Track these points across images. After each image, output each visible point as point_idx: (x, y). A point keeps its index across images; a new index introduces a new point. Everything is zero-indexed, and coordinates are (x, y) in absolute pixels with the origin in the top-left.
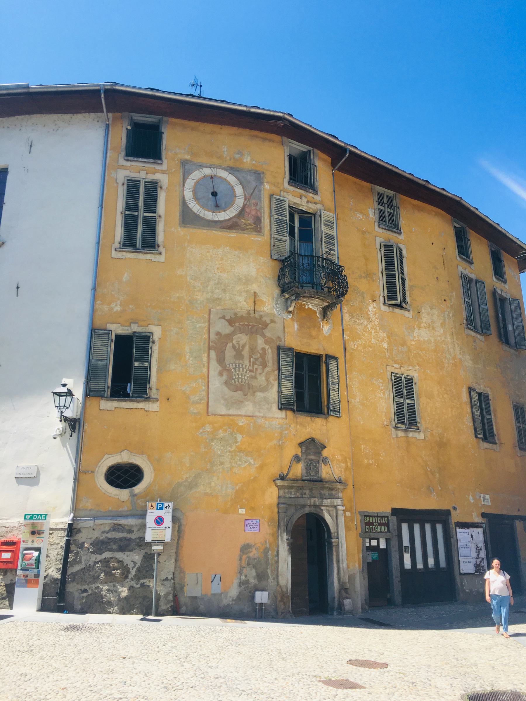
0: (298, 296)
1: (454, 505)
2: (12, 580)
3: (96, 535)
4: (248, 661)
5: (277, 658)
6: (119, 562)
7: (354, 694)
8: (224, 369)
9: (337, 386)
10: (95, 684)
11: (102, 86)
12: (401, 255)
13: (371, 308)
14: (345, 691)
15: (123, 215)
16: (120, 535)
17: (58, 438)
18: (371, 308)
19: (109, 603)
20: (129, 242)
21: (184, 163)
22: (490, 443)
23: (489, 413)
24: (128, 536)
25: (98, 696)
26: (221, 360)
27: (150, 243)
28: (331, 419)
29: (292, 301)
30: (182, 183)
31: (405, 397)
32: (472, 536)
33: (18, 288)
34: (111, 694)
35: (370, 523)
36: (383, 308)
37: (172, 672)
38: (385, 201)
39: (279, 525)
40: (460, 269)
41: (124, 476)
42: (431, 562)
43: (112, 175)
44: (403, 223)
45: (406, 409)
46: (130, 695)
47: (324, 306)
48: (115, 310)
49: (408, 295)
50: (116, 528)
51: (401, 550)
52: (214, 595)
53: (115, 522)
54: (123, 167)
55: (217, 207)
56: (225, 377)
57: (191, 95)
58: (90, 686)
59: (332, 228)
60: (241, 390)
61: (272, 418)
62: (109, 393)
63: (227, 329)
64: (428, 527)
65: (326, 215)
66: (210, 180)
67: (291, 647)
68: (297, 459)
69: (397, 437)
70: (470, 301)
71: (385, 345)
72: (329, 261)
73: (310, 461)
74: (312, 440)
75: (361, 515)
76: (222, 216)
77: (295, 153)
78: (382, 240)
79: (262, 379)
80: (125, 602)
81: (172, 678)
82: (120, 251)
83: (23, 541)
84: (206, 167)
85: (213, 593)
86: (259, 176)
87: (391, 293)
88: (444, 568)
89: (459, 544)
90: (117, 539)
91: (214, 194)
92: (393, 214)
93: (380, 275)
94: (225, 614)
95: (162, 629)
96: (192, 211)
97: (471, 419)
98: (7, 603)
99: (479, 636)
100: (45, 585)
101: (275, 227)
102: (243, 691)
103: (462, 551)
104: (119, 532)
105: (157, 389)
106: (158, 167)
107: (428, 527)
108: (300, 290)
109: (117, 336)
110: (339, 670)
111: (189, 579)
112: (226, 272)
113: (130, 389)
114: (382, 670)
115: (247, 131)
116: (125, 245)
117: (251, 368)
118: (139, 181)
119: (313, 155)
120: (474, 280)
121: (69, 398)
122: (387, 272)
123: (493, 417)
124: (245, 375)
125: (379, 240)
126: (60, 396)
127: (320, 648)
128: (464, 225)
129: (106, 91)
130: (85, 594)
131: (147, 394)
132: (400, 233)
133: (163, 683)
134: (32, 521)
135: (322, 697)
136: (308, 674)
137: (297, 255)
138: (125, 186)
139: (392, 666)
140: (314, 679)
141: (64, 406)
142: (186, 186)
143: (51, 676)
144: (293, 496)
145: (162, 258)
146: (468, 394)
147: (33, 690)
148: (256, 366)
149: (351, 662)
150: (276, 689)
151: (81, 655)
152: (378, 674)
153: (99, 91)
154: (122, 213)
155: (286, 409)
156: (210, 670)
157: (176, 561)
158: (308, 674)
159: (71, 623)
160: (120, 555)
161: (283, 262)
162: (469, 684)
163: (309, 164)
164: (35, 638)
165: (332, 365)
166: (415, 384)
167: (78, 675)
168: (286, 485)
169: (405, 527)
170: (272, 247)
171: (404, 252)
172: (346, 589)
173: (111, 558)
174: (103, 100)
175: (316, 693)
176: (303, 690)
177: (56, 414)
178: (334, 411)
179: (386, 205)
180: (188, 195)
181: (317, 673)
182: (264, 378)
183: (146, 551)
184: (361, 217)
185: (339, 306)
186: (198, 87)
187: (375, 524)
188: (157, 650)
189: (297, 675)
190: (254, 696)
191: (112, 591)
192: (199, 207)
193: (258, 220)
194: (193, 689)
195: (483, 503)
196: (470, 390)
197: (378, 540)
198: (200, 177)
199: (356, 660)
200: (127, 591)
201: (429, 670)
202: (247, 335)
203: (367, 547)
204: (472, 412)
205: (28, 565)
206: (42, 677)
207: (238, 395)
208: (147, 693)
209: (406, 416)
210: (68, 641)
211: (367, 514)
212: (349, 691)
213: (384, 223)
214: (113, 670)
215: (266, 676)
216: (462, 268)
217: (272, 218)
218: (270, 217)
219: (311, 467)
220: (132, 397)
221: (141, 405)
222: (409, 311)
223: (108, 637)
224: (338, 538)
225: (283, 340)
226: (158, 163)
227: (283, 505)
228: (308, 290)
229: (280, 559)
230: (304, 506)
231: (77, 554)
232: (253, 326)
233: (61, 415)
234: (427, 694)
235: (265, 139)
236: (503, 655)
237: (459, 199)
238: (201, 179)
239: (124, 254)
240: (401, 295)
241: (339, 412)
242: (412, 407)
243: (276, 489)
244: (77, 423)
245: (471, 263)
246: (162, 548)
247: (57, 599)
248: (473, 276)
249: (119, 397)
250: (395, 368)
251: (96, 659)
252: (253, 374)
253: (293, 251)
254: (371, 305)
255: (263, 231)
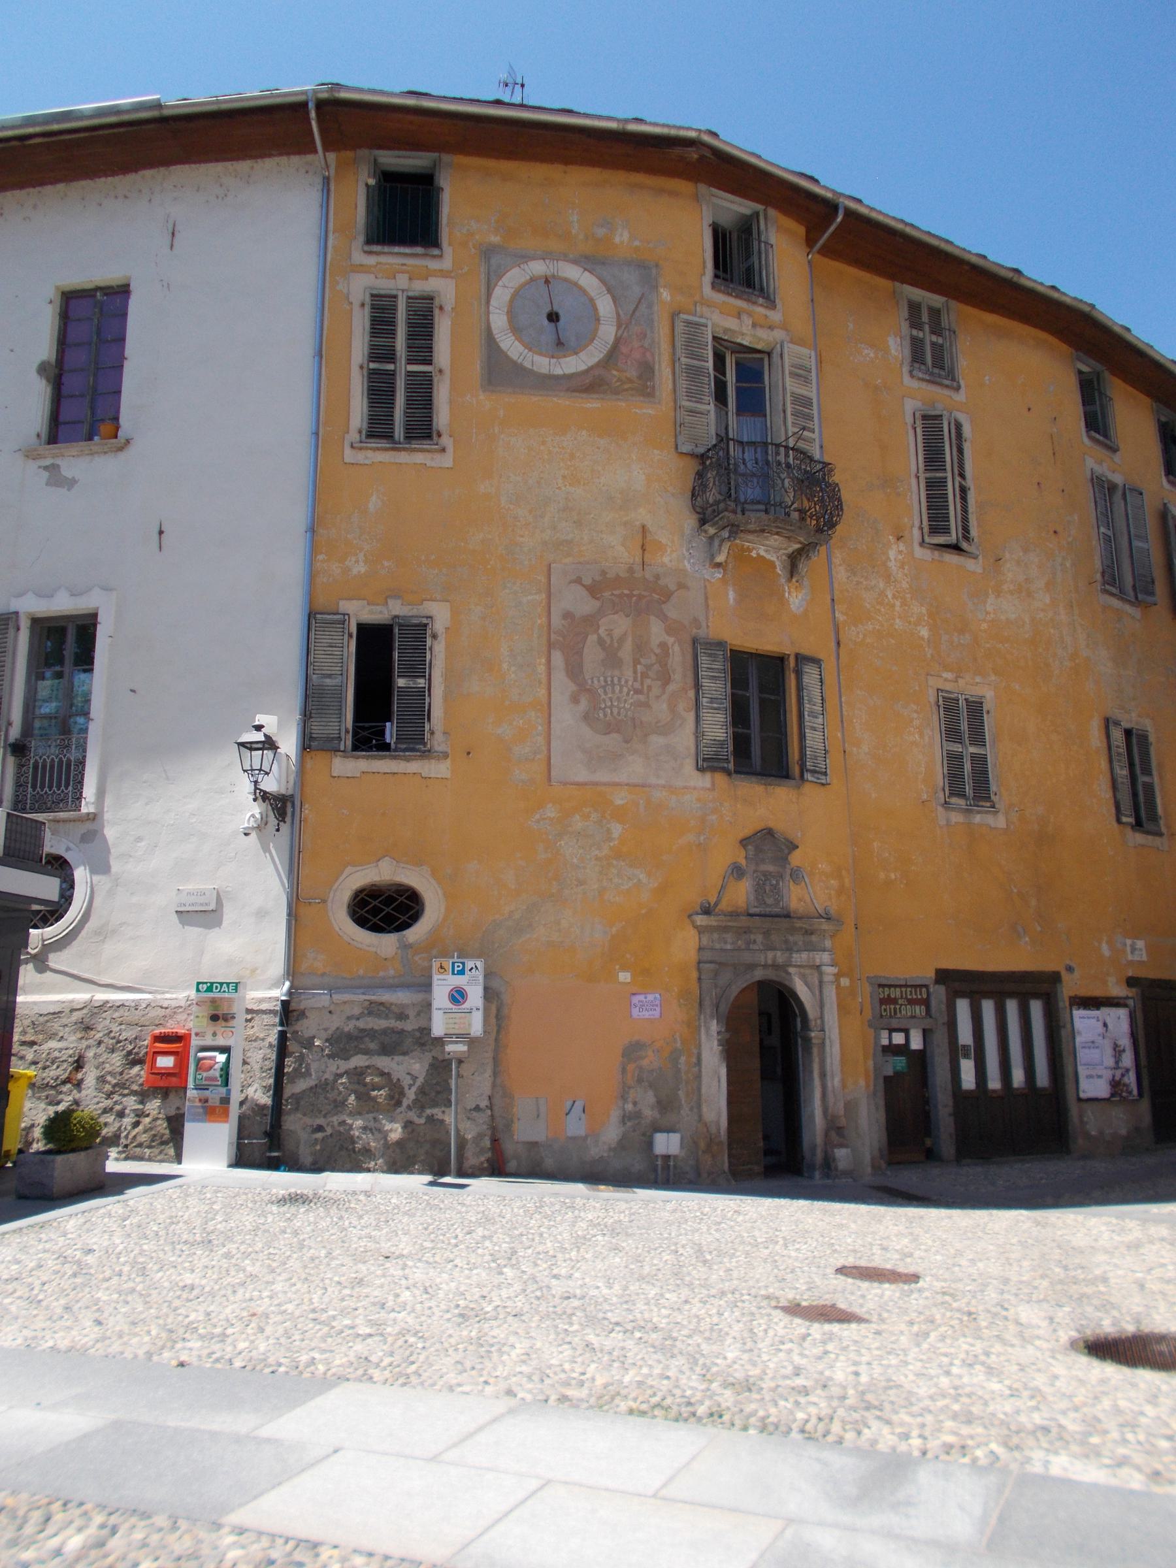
0: (735, 530)
1: (1068, 962)
2: (178, 1108)
3: (335, 1023)
4: (633, 1266)
5: (693, 1262)
6: (382, 1074)
7: (846, 1333)
8: (582, 688)
9: (820, 720)
10: (323, 1306)
11: (310, 95)
12: (959, 435)
13: (894, 553)
14: (827, 1327)
15: (365, 371)
16: (380, 1024)
17: (254, 835)
18: (894, 553)
19: (367, 1152)
20: (378, 429)
21: (487, 252)
22: (1148, 833)
23: (1147, 771)
24: (399, 1025)
25: (326, 1329)
26: (574, 671)
27: (422, 429)
28: (807, 788)
29: (723, 541)
30: (484, 297)
31: (967, 742)
32: (1105, 1025)
33: (161, 532)
34: (353, 1328)
35: (889, 999)
36: (919, 552)
37: (478, 1286)
38: (925, 318)
39: (701, 1004)
40: (1090, 463)
41: (386, 909)
42: (1018, 1077)
43: (340, 287)
44: (963, 364)
45: (968, 767)
46: (389, 1330)
47: (790, 550)
48: (355, 571)
49: (975, 523)
50: (375, 1009)
51: (955, 1052)
52: (574, 1139)
53: (373, 998)
54: (362, 269)
55: (560, 345)
56: (584, 704)
57: (498, 102)
58: (314, 1311)
59: (807, 381)
60: (618, 731)
61: (685, 787)
62: (349, 743)
63: (585, 606)
64: (1012, 1007)
65: (794, 354)
66: (544, 288)
67: (723, 1240)
68: (737, 871)
69: (948, 824)
70: (1110, 533)
71: (924, 632)
72: (801, 453)
73: (765, 876)
74: (769, 833)
75: (871, 984)
76: (572, 364)
77: (726, 221)
78: (919, 404)
79: (661, 709)
80: (398, 1151)
81: (476, 1297)
82: (361, 449)
83: (197, 1034)
84: (534, 258)
85: (569, 1134)
86: (648, 270)
87: (937, 521)
88: (1044, 1089)
89: (1078, 1040)
90: (376, 1031)
91: (553, 317)
92: (942, 346)
93: (914, 481)
94: (594, 1175)
95: (467, 1203)
96: (507, 357)
97: (1109, 784)
98: (172, 1152)
99: (1114, 1221)
100: (241, 1118)
101: (683, 384)
102: (617, 1324)
103: (1083, 1055)
104: (379, 1016)
105: (445, 733)
106: (433, 265)
107: (1012, 1007)
108: (739, 516)
109: (361, 627)
110: (818, 1287)
111: (523, 1107)
112: (577, 489)
113: (390, 732)
114: (906, 1287)
115: (620, 176)
116: (371, 435)
117: (637, 685)
118: (395, 297)
119: (766, 224)
120: (1121, 485)
121: (269, 754)
122: (929, 475)
123: (1156, 780)
124: (625, 701)
125: (910, 405)
126: (251, 749)
127: (781, 1242)
128: (1099, 367)
129: (321, 105)
130: (319, 1135)
131: (425, 744)
132: (958, 388)
133: (458, 1306)
134: (210, 995)
135: (777, 1338)
136: (753, 1291)
137: (731, 443)
138: (367, 309)
139: (927, 1279)
140: (764, 1303)
141: (260, 770)
142: (493, 302)
143: (241, 1291)
144: (729, 947)
145: (447, 460)
146: (1103, 731)
147: (201, 1318)
148: (648, 682)
149: (842, 1271)
150: (685, 1323)
151: (305, 1250)
152: (897, 1295)
153: (304, 105)
154: (361, 367)
155: (713, 769)
156: (554, 1282)
157: (495, 1074)
158: (753, 1291)
159: (293, 1190)
160: (383, 1062)
161: (702, 458)
162: (1086, 1318)
163: (756, 243)
164: (219, 1218)
165: (811, 676)
166: (988, 712)
167: (294, 1289)
168: (715, 924)
169: (963, 1007)
170: (678, 425)
171: (967, 430)
172: (839, 1128)
173: (368, 1067)
174: (314, 124)
175: (766, 1331)
176: (741, 1325)
177: (246, 786)
178: (814, 772)
179: (927, 328)
180: (499, 321)
181: (771, 1290)
182: (665, 706)
183: (434, 1053)
184: (872, 355)
185: (823, 549)
186: (518, 88)
187: (900, 1002)
188: (453, 1241)
189: (730, 1296)
190: (638, 1335)
191: (371, 1130)
192: (521, 348)
193: (647, 370)
194: (516, 1319)
195: (1130, 957)
196: (1108, 723)
197: (906, 1032)
198: (523, 280)
199: (855, 1267)
200: (400, 1130)
201: (1006, 1288)
202: (627, 616)
203: (884, 1046)
204: (1112, 769)
205: (207, 1079)
206: (223, 1292)
207: (613, 741)
208: (425, 1327)
209: (969, 782)
210: (282, 1224)
211: (884, 982)
212: (835, 1327)
213: (923, 367)
214: (362, 1280)
215: (668, 1296)
216: (1095, 461)
217: (677, 365)
218: (674, 363)
219: (766, 886)
220: (395, 750)
221: (414, 766)
222: (976, 558)
223: (361, 1217)
224: (823, 1030)
225: (704, 624)
226: (434, 257)
227: (708, 965)
228: (755, 518)
229: (703, 1070)
230: (752, 967)
231: (301, 1059)
232: (640, 597)
233: (256, 789)
234: (997, 1336)
235: (661, 191)
236: (1162, 1261)
237: (1087, 309)
238: (523, 286)
239: (370, 453)
240: (960, 523)
241: (825, 774)
242: (980, 762)
243: (693, 932)
244: (289, 805)
245: (1114, 450)
246: (465, 1048)
247: (266, 1144)
248: (1118, 479)
249: (370, 749)
250: (946, 680)
251: (333, 1259)
252: (642, 698)
253: (723, 435)
254: (895, 547)
255: (657, 393)
